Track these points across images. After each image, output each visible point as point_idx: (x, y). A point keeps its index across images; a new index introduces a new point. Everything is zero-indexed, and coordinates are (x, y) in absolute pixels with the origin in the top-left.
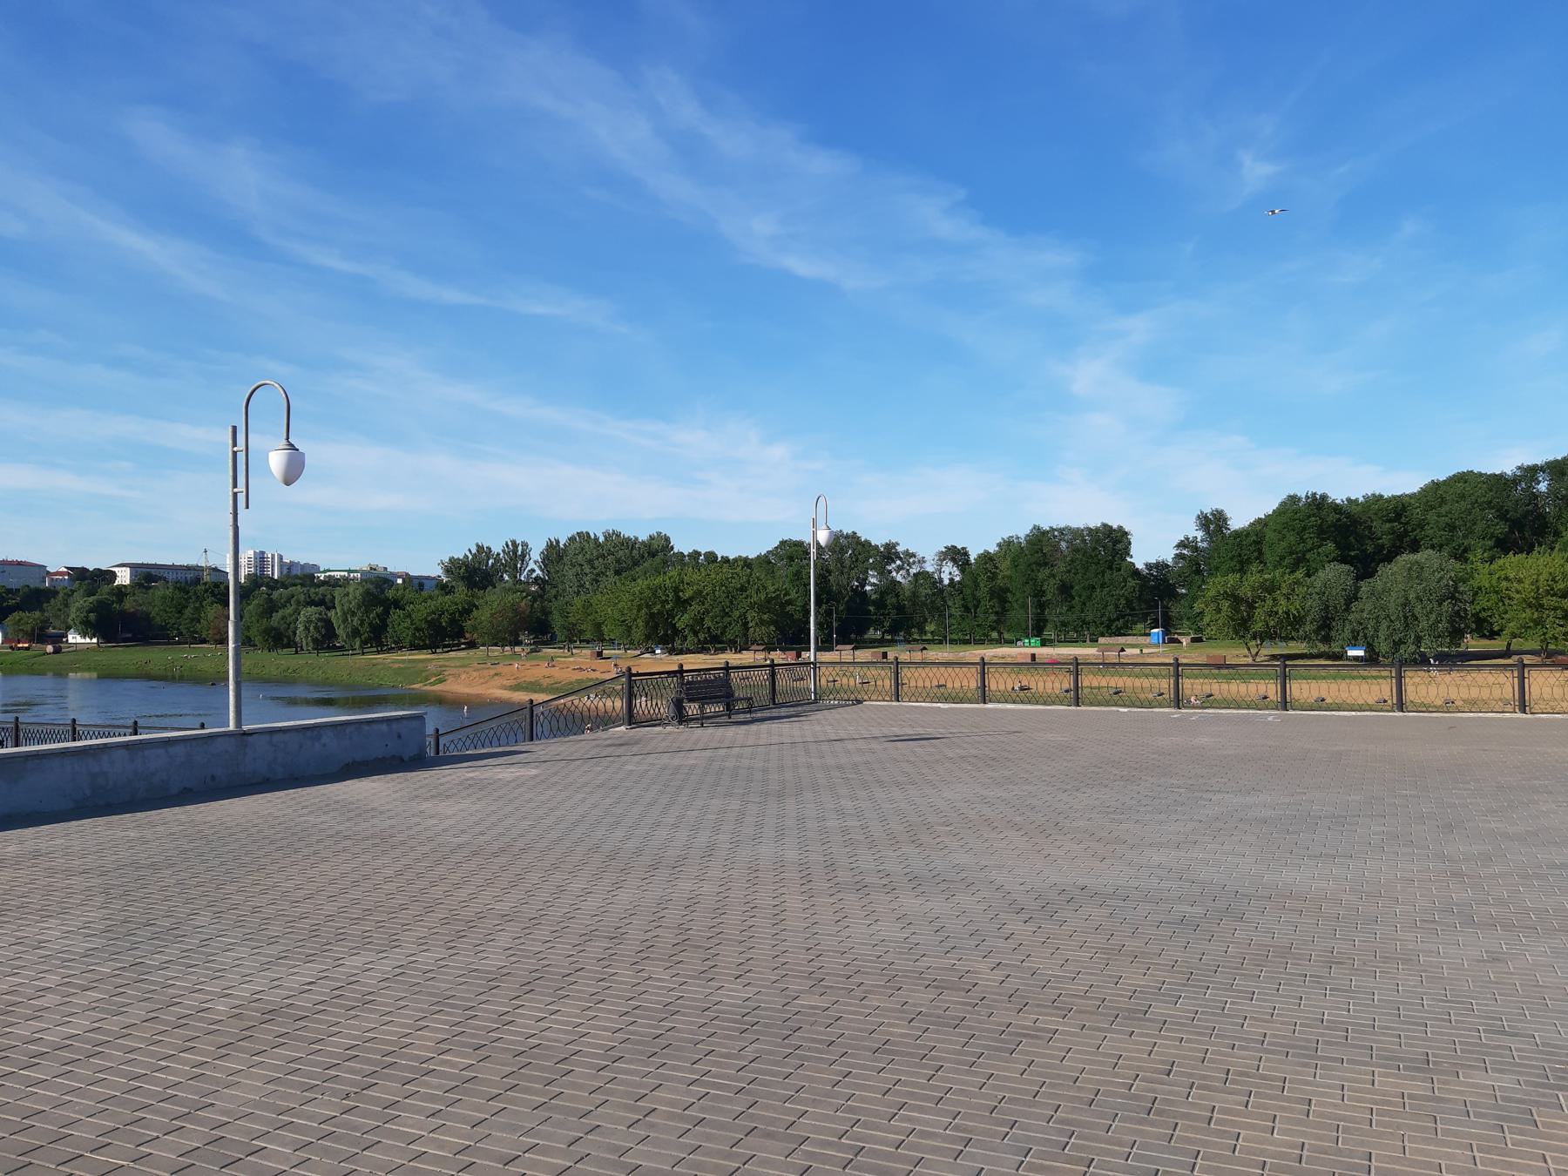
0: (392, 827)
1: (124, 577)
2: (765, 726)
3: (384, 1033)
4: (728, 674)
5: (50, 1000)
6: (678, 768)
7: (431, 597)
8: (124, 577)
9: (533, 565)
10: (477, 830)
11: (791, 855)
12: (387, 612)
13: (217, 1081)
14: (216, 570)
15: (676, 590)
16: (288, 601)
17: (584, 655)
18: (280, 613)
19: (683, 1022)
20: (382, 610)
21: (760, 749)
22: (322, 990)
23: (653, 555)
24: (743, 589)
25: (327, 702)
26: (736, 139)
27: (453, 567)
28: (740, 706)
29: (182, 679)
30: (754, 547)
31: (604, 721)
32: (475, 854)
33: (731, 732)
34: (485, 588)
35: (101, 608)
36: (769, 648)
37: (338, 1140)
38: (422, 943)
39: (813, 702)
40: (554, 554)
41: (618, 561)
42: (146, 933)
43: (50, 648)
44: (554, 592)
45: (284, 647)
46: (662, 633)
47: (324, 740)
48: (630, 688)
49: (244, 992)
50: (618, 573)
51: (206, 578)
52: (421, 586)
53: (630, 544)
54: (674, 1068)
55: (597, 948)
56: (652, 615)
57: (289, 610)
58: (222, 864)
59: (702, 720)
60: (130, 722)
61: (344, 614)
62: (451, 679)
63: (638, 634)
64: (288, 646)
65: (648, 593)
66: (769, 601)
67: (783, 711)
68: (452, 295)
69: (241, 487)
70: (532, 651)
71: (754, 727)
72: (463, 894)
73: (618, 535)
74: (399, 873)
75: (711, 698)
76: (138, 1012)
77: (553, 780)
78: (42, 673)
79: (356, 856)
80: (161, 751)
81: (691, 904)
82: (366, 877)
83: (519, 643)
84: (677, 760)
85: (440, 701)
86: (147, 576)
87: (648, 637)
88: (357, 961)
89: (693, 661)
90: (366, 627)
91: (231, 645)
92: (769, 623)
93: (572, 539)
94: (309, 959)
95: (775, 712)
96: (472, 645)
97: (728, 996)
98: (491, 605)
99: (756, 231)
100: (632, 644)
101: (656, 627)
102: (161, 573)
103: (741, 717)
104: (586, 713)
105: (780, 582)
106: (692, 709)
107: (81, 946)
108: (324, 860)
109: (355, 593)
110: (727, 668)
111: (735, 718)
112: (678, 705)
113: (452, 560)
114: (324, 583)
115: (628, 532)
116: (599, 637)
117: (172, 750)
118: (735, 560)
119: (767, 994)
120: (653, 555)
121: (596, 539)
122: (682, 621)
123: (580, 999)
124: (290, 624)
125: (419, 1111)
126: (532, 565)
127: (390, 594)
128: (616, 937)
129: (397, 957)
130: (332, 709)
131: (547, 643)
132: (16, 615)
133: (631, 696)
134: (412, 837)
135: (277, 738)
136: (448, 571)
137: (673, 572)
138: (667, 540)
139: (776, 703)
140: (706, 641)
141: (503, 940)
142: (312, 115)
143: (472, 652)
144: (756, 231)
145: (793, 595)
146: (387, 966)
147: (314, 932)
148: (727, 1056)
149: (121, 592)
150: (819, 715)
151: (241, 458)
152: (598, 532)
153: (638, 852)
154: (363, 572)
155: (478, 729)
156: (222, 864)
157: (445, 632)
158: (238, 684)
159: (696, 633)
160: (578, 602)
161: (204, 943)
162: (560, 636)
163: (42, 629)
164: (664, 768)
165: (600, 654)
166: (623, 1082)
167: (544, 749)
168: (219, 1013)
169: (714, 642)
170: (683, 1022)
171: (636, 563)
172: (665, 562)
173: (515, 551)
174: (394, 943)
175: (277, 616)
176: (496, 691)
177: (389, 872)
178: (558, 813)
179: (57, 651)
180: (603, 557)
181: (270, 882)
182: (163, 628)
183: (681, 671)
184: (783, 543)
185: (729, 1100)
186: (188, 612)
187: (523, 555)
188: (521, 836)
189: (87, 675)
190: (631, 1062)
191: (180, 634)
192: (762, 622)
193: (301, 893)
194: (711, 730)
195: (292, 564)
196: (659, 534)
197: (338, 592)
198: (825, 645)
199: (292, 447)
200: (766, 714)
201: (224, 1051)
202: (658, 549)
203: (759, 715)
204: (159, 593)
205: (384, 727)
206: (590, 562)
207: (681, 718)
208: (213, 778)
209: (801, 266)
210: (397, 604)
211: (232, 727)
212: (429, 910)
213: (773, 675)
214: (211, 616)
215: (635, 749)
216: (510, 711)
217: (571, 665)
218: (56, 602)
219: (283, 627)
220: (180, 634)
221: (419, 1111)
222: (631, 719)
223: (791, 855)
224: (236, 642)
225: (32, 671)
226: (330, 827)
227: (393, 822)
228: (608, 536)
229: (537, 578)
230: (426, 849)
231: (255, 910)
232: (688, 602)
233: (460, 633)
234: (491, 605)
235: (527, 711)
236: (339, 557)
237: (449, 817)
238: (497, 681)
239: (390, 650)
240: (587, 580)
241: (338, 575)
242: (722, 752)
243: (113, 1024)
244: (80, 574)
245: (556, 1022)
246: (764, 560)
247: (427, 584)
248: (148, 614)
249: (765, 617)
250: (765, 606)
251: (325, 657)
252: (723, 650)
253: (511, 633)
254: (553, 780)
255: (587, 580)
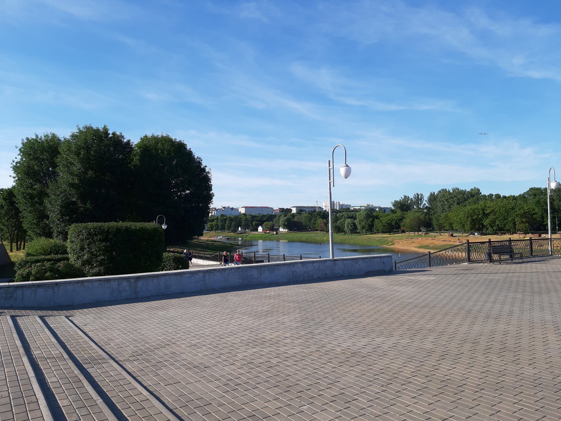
0: (385, 294)
1: (294, 211)
2: (529, 265)
3: (392, 366)
4: (510, 243)
5: (288, 341)
6: (491, 281)
7: (388, 215)
8: (294, 211)
9: (425, 202)
10: (415, 298)
11: (548, 317)
12: (373, 220)
13: (340, 374)
14: (320, 207)
15: (483, 210)
16: (342, 217)
17: (445, 236)
18: (340, 221)
19: (508, 379)
20: (371, 220)
21: (528, 274)
22: (369, 349)
23: (473, 196)
24: (513, 209)
25: (356, 251)
26: (503, 29)
27: (396, 204)
28: (516, 256)
29: (311, 242)
30: (518, 191)
31: (458, 261)
32: (416, 306)
33: (513, 266)
34: (407, 211)
35: (288, 220)
36: (526, 233)
37: (382, 400)
38: (401, 336)
39: (545, 256)
40: (433, 198)
41: (458, 199)
42: (312, 323)
43: (275, 233)
44: (433, 212)
45: (341, 232)
46: (477, 226)
47: (359, 263)
48: (469, 248)
49: (345, 345)
50: (458, 204)
51: (317, 210)
52: (385, 211)
53: (463, 193)
54: (506, 396)
55: (468, 346)
56: (473, 220)
57: (342, 220)
58: (332, 302)
59: (500, 261)
60: (299, 256)
61: (360, 221)
62: (396, 244)
63: (468, 227)
64: (342, 232)
65: (471, 211)
66: (525, 213)
67: (537, 259)
68: (393, 107)
69: (332, 180)
70: (425, 234)
71: (524, 265)
72: (413, 320)
73: (458, 189)
74: (390, 311)
75: (505, 252)
76: (313, 348)
77: (442, 281)
78: (273, 240)
79: (374, 303)
80: (311, 265)
81: (506, 333)
82: (379, 311)
83: (421, 231)
84: (491, 277)
85: (392, 251)
86: (301, 210)
87: (471, 229)
88: (379, 340)
89: (494, 238)
90: (367, 226)
91: (330, 231)
92: (525, 223)
93: (440, 192)
94: (364, 337)
95: (533, 259)
96: (403, 232)
97: (526, 372)
98: (410, 217)
99: (515, 64)
100: (465, 231)
101: (475, 224)
102: (304, 209)
103: (517, 261)
104: (448, 257)
105: (531, 205)
106: (495, 257)
107: (295, 325)
108: (364, 304)
109: (363, 214)
110: (510, 241)
111: (514, 261)
112: (490, 255)
113: (396, 202)
114: (353, 211)
115: (462, 188)
116: (451, 229)
117: (314, 265)
118: (509, 197)
119: (544, 373)
120: (473, 196)
121: (449, 191)
122: (486, 222)
123: (464, 364)
124: (343, 225)
125: (409, 396)
126: (424, 202)
127: (375, 214)
128: (475, 343)
129: (392, 340)
130: (357, 253)
131: (431, 231)
132: (266, 223)
133: (469, 252)
134: (392, 299)
135: (345, 262)
136: (394, 205)
137: (481, 203)
138: (479, 190)
139: (532, 255)
140: (497, 230)
141: (431, 339)
142: (354, 57)
143: (403, 234)
144: (515, 64)
145: (537, 210)
146: (390, 343)
147: (364, 328)
148: (530, 395)
149: (293, 215)
150: (554, 261)
151: (331, 170)
152: (450, 189)
153: (480, 311)
154: (365, 207)
155: (410, 261)
156: (332, 302)
157: (394, 227)
158: (332, 244)
159: (492, 227)
160: (443, 215)
161: (330, 328)
162: (436, 228)
163: (273, 227)
164: (486, 280)
165: (452, 235)
166: (485, 398)
167: (436, 270)
168: (338, 351)
169: (501, 230)
170: (508, 379)
171: (466, 200)
172: (478, 199)
173: (418, 197)
174: (391, 335)
175: (338, 222)
176: (413, 248)
177: (386, 310)
178: (445, 294)
179: (277, 234)
180: (452, 198)
181: (348, 310)
182: (305, 226)
183: (490, 242)
184: (531, 189)
185: (533, 413)
186: (312, 221)
187: (421, 199)
188: (432, 301)
189: (285, 241)
190: (488, 391)
191: (310, 228)
192: (522, 222)
193: (358, 315)
194: (504, 266)
195: (343, 205)
196: (475, 188)
197: (357, 214)
198: (554, 231)
199: (347, 166)
200: (529, 260)
201: (341, 364)
202: (475, 194)
203: (525, 260)
204: (304, 215)
205: (379, 260)
206: (447, 200)
207: (491, 260)
208: (326, 274)
209: (536, 74)
210: (377, 217)
211: (331, 258)
212: (402, 325)
213: (531, 244)
214: (319, 222)
215: (473, 271)
216: (421, 256)
217: (439, 240)
218: (276, 219)
219: (340, 226)
220: (310, 228)
221: (409, 396)
222: (469, 260)
223: (548, 317)
224: (331, 230)
225: (271, 240)
226: (364, 293)
227: (385, 293)
228: (454, 190)
229: (427, 207)
230: (398, 303)
231: (345, 319)
232: (488, 215)
233: (399, 227)
234: (410, 217)
235: (428, 256)
236: (357, 202)
237: (403, 293)
238: (413, 245)
239: (375, 233)
240: (446, 207)
241: (357, 208)
242: (510, 275)
243: (307, 351)
244: (282, 210)
245: (455, 372)
246: (523, 197)
247: (387, 210)
248: (301, 222)
249: (524, 220)
250: (522, 216)
251: (354, 236)
252: (505, 234)
253: (417, 227)
254: (442, 281)
255: (446, 207)
